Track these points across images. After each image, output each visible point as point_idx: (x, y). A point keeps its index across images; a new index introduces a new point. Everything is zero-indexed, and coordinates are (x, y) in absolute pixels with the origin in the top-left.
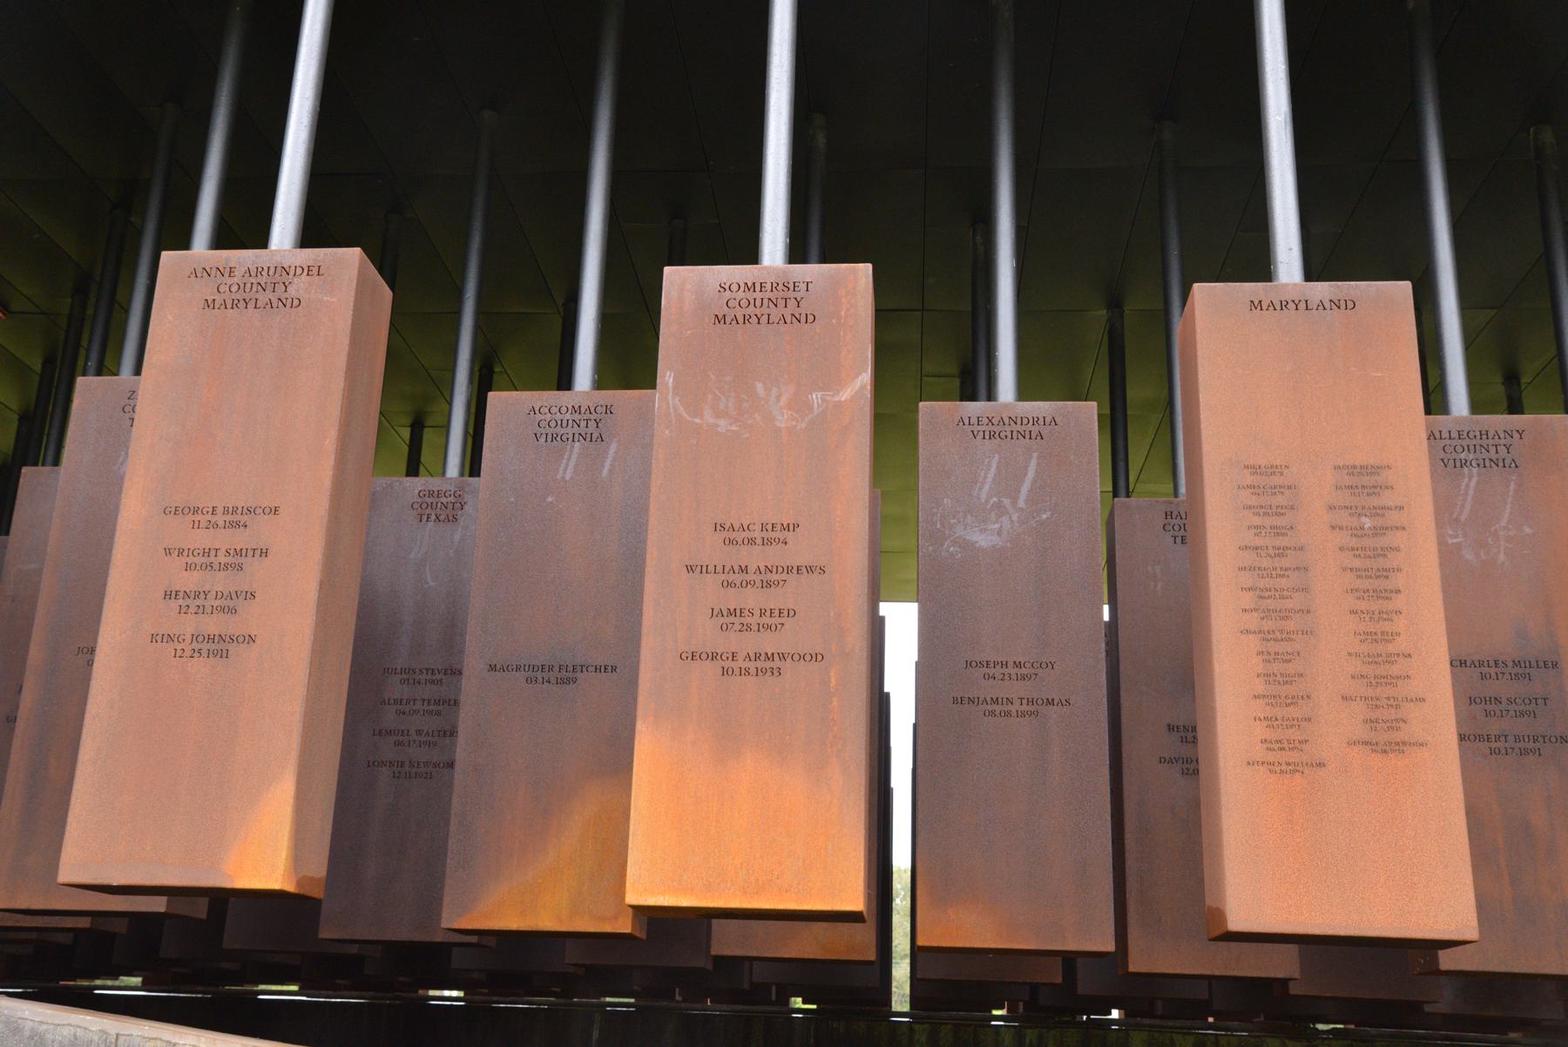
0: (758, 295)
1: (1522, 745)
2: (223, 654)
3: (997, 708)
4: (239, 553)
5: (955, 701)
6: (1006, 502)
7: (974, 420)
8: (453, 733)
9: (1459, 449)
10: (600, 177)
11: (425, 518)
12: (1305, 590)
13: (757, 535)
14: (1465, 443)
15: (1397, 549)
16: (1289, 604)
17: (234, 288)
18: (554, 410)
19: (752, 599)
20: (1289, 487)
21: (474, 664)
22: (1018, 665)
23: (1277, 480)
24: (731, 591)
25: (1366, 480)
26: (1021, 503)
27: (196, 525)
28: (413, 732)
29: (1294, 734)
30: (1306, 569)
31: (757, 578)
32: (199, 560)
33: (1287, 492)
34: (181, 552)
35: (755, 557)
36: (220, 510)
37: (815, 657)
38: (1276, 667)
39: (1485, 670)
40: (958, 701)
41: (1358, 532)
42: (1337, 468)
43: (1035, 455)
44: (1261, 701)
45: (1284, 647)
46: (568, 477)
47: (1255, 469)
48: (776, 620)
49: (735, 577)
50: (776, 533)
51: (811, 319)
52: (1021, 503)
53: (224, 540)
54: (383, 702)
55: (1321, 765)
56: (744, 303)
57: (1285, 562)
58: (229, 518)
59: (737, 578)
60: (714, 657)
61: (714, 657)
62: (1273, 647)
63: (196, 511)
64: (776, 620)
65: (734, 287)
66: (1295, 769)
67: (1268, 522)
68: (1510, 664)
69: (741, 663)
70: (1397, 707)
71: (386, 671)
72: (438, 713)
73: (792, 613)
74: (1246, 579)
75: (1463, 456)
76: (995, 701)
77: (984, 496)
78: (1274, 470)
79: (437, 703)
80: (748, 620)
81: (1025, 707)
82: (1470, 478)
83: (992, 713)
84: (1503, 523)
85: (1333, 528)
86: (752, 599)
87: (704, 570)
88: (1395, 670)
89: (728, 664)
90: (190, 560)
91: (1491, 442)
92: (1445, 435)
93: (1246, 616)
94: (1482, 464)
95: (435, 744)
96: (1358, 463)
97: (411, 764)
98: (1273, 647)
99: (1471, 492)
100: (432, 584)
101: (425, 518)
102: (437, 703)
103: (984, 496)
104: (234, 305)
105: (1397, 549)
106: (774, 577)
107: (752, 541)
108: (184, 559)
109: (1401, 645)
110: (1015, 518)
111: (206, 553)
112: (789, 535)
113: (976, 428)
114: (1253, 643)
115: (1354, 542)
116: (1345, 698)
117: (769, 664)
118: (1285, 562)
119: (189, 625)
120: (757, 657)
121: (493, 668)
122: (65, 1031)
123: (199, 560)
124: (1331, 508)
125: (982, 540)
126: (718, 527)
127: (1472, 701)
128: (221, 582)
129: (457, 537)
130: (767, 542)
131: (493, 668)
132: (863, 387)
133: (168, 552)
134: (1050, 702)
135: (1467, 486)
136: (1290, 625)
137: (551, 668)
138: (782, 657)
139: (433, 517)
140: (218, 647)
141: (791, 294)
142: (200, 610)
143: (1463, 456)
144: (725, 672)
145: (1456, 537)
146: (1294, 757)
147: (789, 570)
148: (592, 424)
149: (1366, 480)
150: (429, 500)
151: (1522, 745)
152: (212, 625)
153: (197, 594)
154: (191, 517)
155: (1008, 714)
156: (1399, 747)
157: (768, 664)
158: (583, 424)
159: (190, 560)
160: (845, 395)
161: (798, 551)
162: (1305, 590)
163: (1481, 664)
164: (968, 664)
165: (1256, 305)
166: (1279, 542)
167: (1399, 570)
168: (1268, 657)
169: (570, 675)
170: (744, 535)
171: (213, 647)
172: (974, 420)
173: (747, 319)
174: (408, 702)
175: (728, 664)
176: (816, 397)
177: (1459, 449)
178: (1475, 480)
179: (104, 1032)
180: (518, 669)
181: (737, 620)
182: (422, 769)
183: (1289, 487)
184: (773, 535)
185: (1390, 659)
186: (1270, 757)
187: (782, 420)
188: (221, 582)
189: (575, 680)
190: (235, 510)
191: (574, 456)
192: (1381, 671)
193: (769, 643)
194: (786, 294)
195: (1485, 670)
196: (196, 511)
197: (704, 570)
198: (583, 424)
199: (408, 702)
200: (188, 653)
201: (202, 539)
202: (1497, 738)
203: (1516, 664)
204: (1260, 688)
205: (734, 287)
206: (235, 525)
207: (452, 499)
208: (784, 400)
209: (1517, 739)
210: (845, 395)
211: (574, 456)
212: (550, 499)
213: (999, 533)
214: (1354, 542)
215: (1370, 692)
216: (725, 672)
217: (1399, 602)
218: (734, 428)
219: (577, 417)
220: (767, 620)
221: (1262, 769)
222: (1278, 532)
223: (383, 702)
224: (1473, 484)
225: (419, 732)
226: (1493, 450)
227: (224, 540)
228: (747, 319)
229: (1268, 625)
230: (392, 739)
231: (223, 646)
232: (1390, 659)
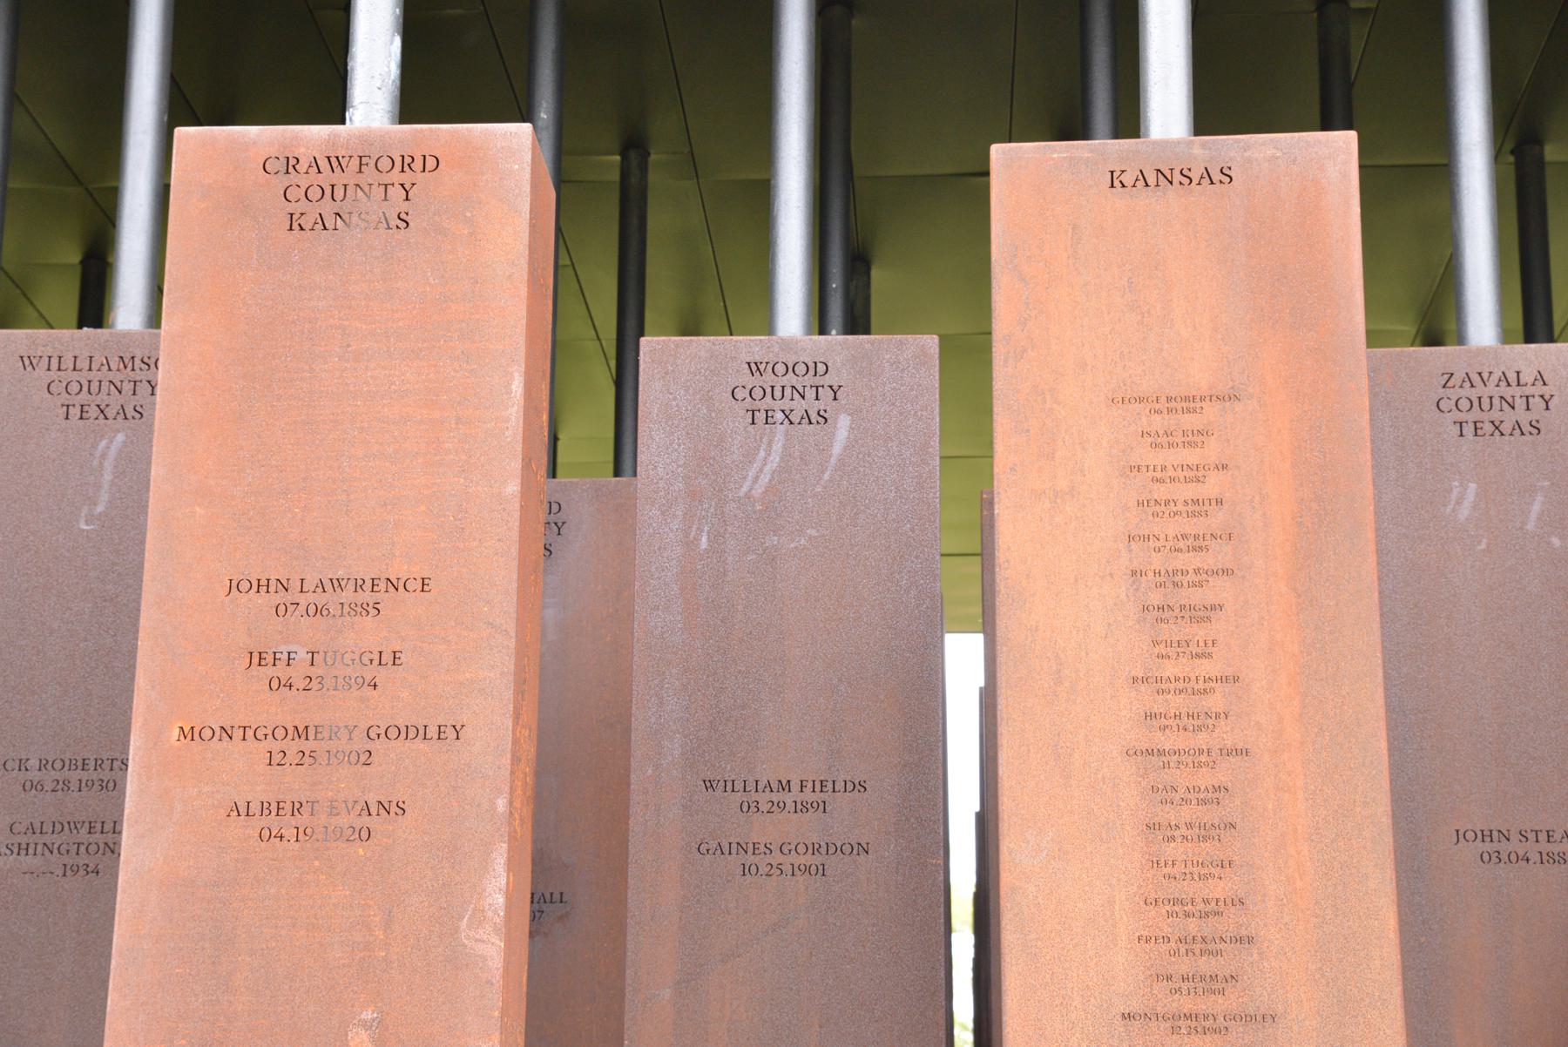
158: (127, 387)
198: (127, 387)
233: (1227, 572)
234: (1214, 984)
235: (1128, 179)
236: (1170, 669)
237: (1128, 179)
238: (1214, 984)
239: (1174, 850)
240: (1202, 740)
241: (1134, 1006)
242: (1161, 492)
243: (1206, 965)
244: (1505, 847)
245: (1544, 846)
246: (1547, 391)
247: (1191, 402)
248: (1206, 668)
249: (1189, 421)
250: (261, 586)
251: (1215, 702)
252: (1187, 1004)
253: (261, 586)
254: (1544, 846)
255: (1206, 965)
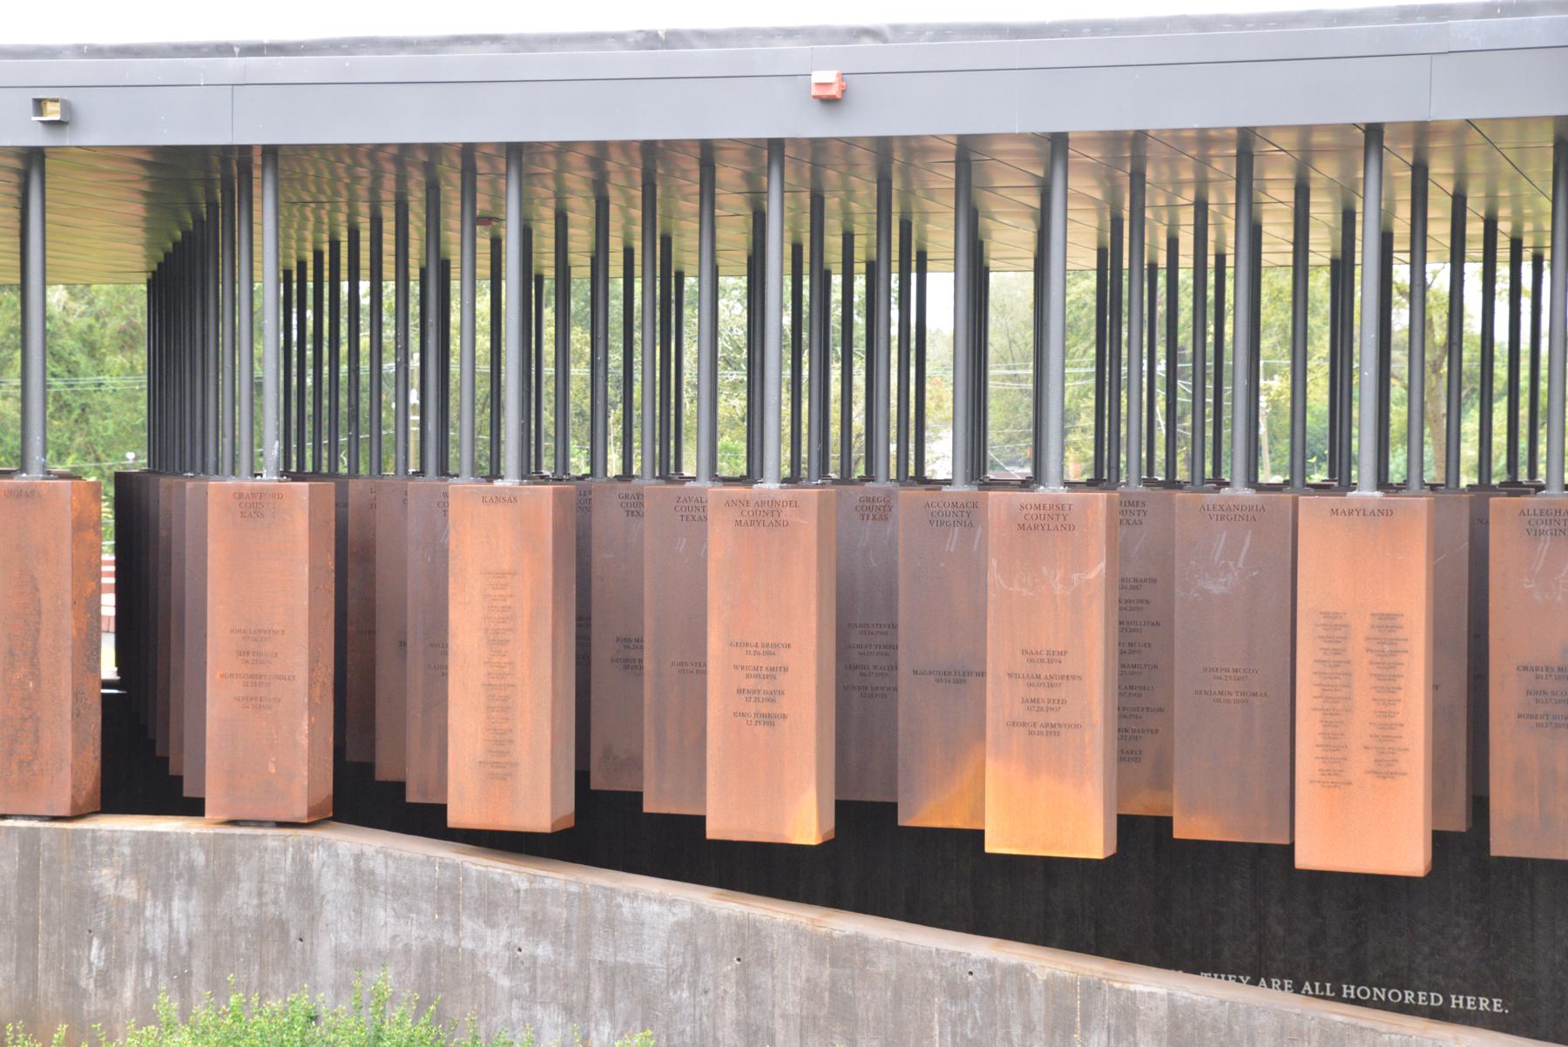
0: (1042, 512)
1: (1557, 721)
2: (772, 724)
3: (1222, 697)
4: (772, 669)
5: (1196, 692)
6: (1231, 563)
7: (1211, 507)
8: (896, 647)
9: (1540, 522)
10: (947, 434)
11: (865, 517)
12: (1348, 686)
13: (1045, 656)
14: (1544, 518)
15: (1402, 664)
16: (1339, 694)
17: (751, 514)
18: (941, 505)
19: (1043, 693)
20: (1345, 626)
21: (904, 670)
22: (1236, 671)
23: (1338, 621)
24: (1032, 688)
25: (1388, 623)
26: (1240, 565)
27: (748, 653)
28: (871, 667)
29: (1336, 767)
30: (1350, 675)
31: (1046, 681)
32: (753, 672)
33: (1343, 629)
34: (743, 668)
35: (1045, 670)
36: (760, 644)
37: (1077, 726)
38: (1330, 730)
39: (1539, 673)
40: (1198, 692)
41: (1382, 653)
42: (1373, 615)
43: (1250, 532)
44: (1322, 748)
45: (1336, 718)
46: (952, 550)
47: (1326, 615)
48: (1056, 706)
49: (1034, 680)
50: (1055, 656)
51: (1072, 528)
52: (1240, 565)
53: (764, 662)
54: (850, 647)
55: (1350, 784)
56: (1034, 517)
57: (1339, 670)
58: (765, 649)
59: (1035, 681)
60: (1024, 724)
61: (1024, 724)
62: (1329, 718)
63: (747, 645)
64: (1056, 706)
65: (1029, 507)
66: (1335, 785)
67: (1331, 646)
68: (1556, 669)
69: (1039, 728)
70: (1393, 753)
71: (850, 625)
72: (887, 654)
73: (1065, 702)
74: (1316, 679)
75: (1542, 527)
76: (1221, 693)
77: (1216, 559)
78: (1336, 615)
79: (885, 647)
80: (1041, 705)
81: (1239, 697)
82: (1545, 542)
83: (1219, 701)
84: (1563, 575)
85: (1367, 650)
86: (1043, 693)
87: (1017, 676)
88: (1394, 733)
89: (1032, 729)
90: (748, 672)
91: (1562, 517)
92: (1531, 512)
93: (1315, 700)
94: (1554, 534)
95: (887, 675)
96: (1386, 612)
97: (872, 689)
98: (1329, 718)
99: (1545, 552)
100: (874, 565)
101: (865, 517)
102: (885, 647)
103: (1216, 559)
104: (752, 523)
105: (1402, 664)
106: (1055, 681)
107: (1042, 661)
108: (745, 672)
109: (1398, 719)
110: (1236, 574)
111: (756, 669)
112: (1062, 658)
113: (1212, 513)
114: (1318, 716)
115: (1379, 659)
116: (1366, 748)
117: (1053, 729)
118: (1339, 670)
119: (751, 708)
120: (1047, 725)
121: (915, 672)
122: (724, 911)
123: (753, 672)
124: (1367, 639)
125: (1216, 589)
126: (1024, 652)
127: (1529, 693)
128: (765, 685)
129: (889, 530)
130: (1050, 661)
131: (915, 672)
132: (1101, 571)
133: (736, 667)
134: (1255, 694)
135: (1543, 548)
136: (1339, 706)
137: (950, 673)
138: (1060, 725)
139: (871, 517)
140: (769, 720)
141: (1060, 512)
142: (757, 700)
143: (1542, 527)
144: (1030, 733)
145: (1530, 583)
146: (1335, 779)
147: (1062, 677)
148: (965, 514)
149: (1388, 623)
150: (867, 504)
151: (1557, 721)
152: (764, 708)
153: (754, 692)
154: (745, 649)
155: (1228, 701)
156: (1392, 775)
157: (1053, 730)
158: (959, 514)
159: (748, 672)
160: (1092, 575)
161: (1068, 667)
162: (1348, 686)
163: (1537, 668)
164: (1205, 670)
165: (1335, 512)
166: (1338, 658)
167: (1402, 676)
168: (1327, 724)
169: (962, 678)
170: (1039, 656)
171: (766, 720)
172: (1211, 507)
173: (1036, 527)
174: (866, 646)
175: (1032, 729)
176: (1075, 577)
177: (1540, 522)
178: (1548, 544)
179: (742, 912)
180: (930, 673)
181: (1036, 705)
182: (880, 692)
183: (1345, 626)
184: (1052, 657)
185: (1392, 727)
186: (1323, 779)
187: (1059, 589)
188: (765, 685)
189: (965, 681)
190: (768, 645)
191: (956, 537)
192: (1386, 733)
193: (1053, 718)
194: (1059, 512)
195: (1539, 673)
196: (747, 645)
197: (1017, 676)
198: (959, 514)
199: (866, 646)
200: (754, 723)
201: (752, 661)
202: (1542, 717)
203: (1560, 669)
204: (1320, 740)
205: (1029, 507)
206: (769, 653)
207: (883, 504)
208: (1058, 578)
209: (1555, 717)
210: (1092, 575)
211: (956, 537)
212: (942, 565)
213: (1226, 584)
214: (1379, 659)
215: (1380, 745)
216: (1030, 733)
217: (1400, 694)
218: (1031, 594)
219: (955, 510)
220: (1051, 705)
221: (1319, 785)
222: (1336, 652)
223: (850, 647)
224: (1546, 547)
225: (875, 667)
226: (1562, 523)
227: (764, 662)
228: (1036, 527)
229: (1327, 706)
230: (858, 671)
231: (771, 720)
232: (1392, 727)
233: (510, 630)
234: (502, 754)
235: (488, 499)
236: (495, 660)
237: (488, 499)
238: (502, 754)
239: (494, 714)
240: (503, 682)
241: (482, 759)
242: (494, 603)
243: (501, 748)
244: (686, 668)
245: (698, 668)
246: (1145, 509)
247: (503, 574)
248: (505, 660)
249: (503, 581)
250: (239, 631)
251: (507, 670)
252: (495, 759)
253: (239, 631)
254: (698, 668)
255: (501, 748)
